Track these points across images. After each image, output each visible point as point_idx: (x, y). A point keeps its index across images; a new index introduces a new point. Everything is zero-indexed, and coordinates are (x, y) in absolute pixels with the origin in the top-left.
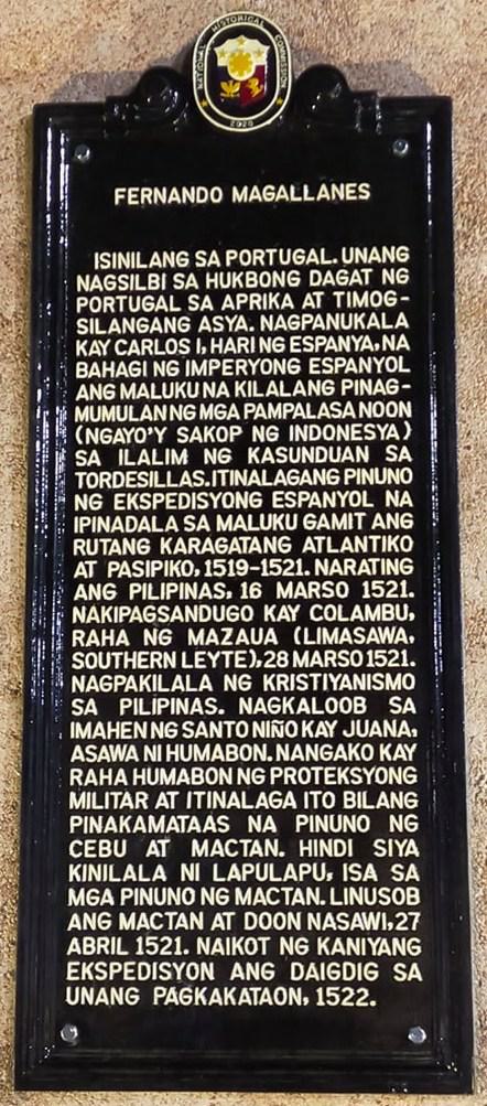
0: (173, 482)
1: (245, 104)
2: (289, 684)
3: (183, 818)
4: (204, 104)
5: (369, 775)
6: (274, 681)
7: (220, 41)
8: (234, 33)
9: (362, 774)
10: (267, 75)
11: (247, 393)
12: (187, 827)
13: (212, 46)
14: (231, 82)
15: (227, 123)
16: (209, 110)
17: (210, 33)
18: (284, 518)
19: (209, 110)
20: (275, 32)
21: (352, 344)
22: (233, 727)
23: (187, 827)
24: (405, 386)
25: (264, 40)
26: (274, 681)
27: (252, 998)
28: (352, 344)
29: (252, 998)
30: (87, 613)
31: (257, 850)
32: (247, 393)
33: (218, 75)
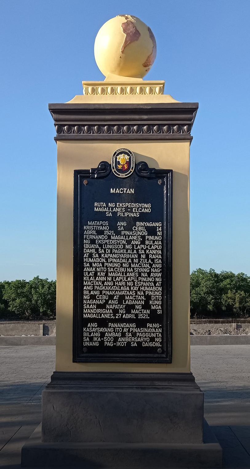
0: (125, 275)
1: (122, 171)
2: (89, 228)
3: (115, 287)
4: (114, 170)
5: (118, 242)
6: (86, 227)
7: (118, 155)
8: (121, 153)
9: (139, 205)
10: (129, 163)
11: (123, 252)
12: (126, 294)
13: (116, 156)
14: (120, 165)
15: (119, 175)
16: (115, 171)
17: (116, 153)
18: (123, 250)
19: (115, 171)
20: (131, 153)
21: (144, 224)
22: (103, 269)
23: (126, 294)
24: (114, 344)
25: (128, 155)
26: (86, 227)
27: (118, 307)
28: (144, 224)
29: (118, 307)
30: (138, 302)
31: (139, 298)
32: (123, 252)
33: (117, 163)
